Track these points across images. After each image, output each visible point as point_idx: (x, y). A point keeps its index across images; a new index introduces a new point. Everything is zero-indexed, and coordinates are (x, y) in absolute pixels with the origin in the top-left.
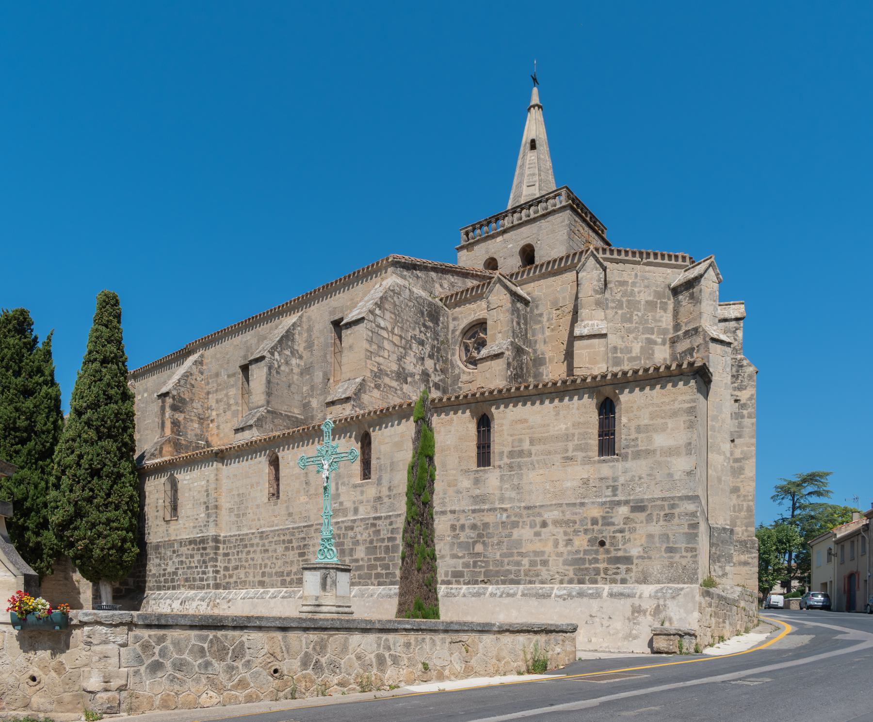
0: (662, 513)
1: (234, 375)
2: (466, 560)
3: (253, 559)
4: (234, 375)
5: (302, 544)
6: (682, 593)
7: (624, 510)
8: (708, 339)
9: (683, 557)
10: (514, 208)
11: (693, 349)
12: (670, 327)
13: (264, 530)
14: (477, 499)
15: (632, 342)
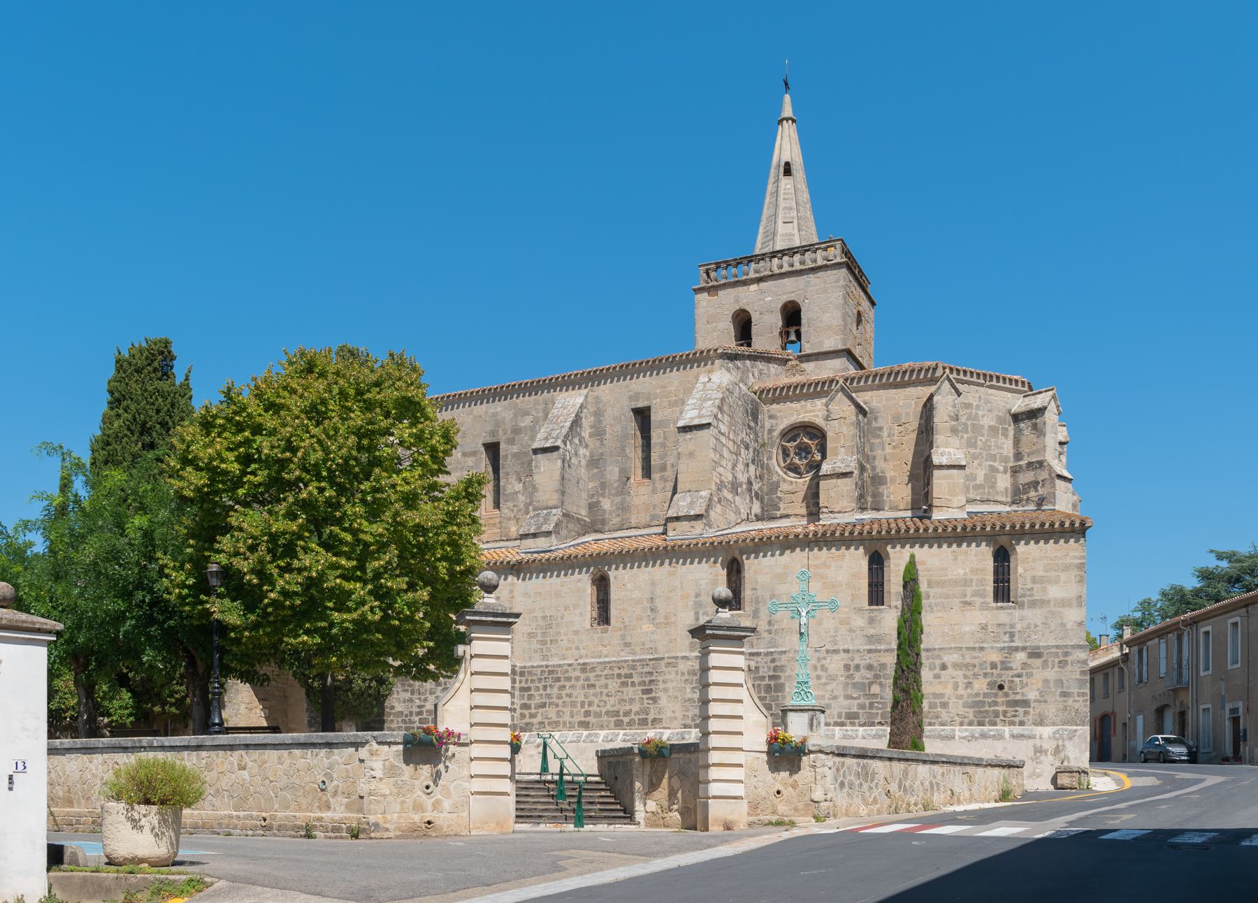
0: (1057, 660)
1: (474, 454)
2: (861, 701)
3: (570, 696)
4: (474, 454)
5: (647, 679)
6: (1077, 734)
7: (1021, 656)
8: (1054, 475)
9: (1076, 701)
10: (774, 252)
11: (1037, 483)
12: (1011, 455)
13: (587, 661)
14: (870, 639)
15: (977, 468)
